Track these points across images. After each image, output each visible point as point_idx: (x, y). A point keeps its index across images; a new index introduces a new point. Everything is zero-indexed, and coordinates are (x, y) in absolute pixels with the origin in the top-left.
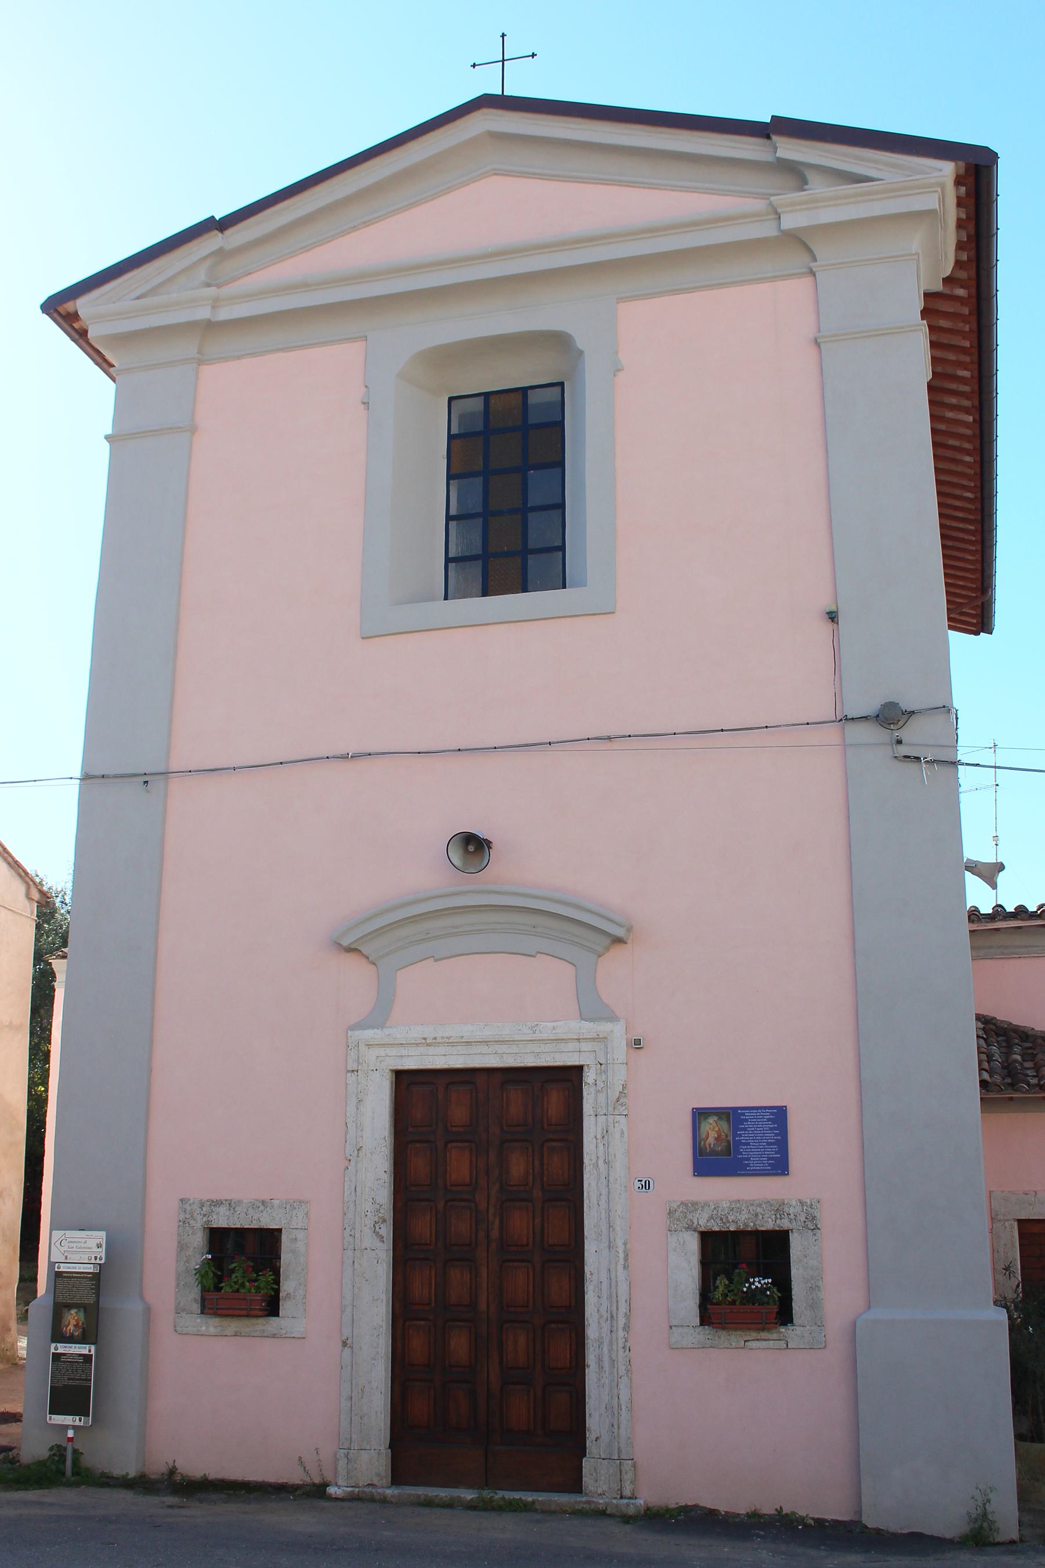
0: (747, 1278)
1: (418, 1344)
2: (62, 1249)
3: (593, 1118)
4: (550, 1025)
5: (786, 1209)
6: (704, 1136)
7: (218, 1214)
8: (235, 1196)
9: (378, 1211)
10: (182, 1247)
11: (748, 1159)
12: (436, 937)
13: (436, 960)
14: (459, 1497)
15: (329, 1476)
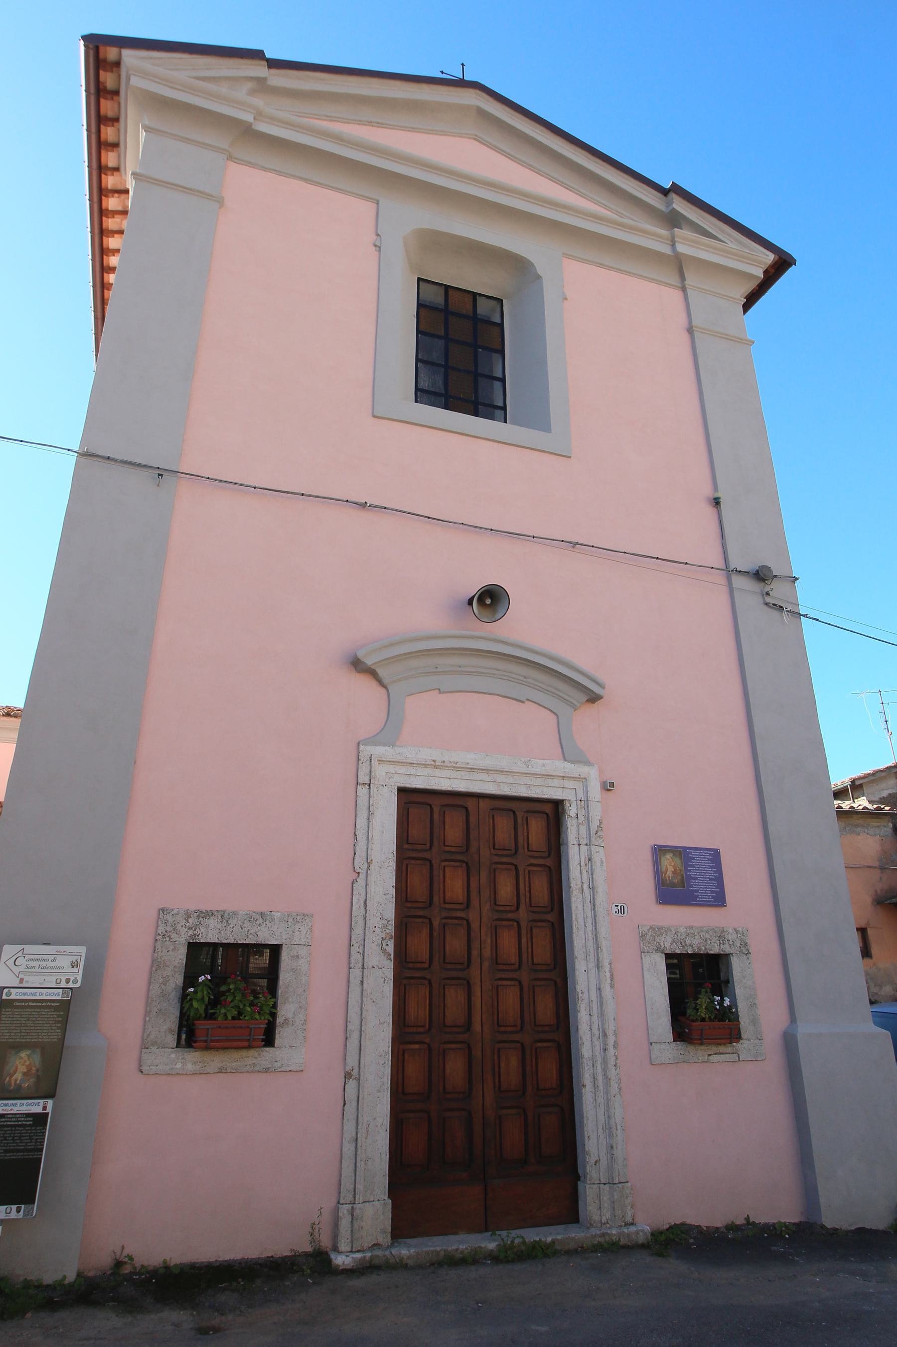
0: (700, 994)
1: (414, 1069)
2: (16, 970)
3: (576, 847)
4: (541, 762)
5: (726, 936)
6: (664, 869)
7: (207, 926)
8: (228, 907)
9: (386, 926)
10: (156, 965)
11: (697, 891)
12: (444, 673)
13: (440, 692)
14: (480, 1247)
15: (325, 1242)
